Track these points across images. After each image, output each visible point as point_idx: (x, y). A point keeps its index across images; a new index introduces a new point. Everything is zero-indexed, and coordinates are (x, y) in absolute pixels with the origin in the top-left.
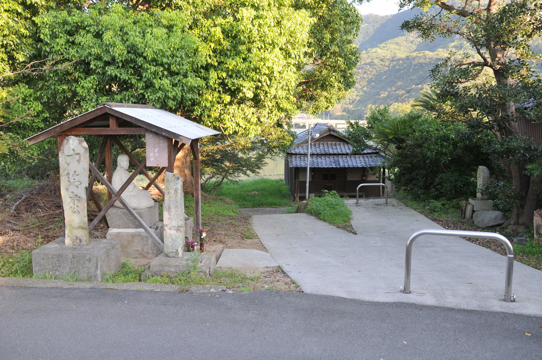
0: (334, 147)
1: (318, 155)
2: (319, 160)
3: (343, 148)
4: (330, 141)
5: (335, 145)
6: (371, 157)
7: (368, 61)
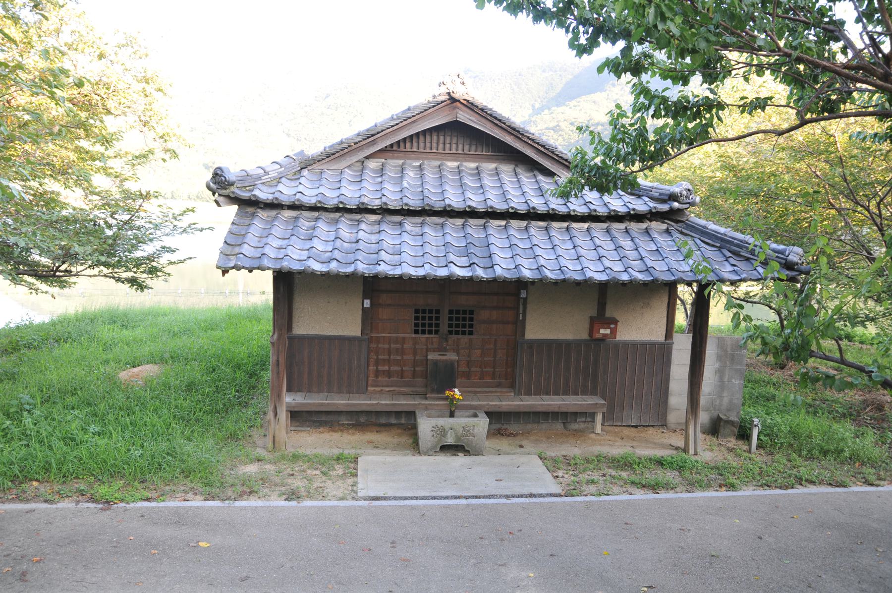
0: (469, 181)
1: (385, 211)
2: (389, 235)
3: (508, 187)
4: (454, 156)
5: (478, 173)
6: (647, 232)
7: (552, 125)
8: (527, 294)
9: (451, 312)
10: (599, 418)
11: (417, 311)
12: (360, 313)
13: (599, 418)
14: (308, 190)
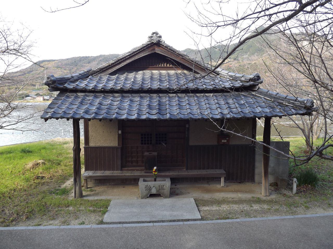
8: (189, 126)
9: (156, 135)
10: (222, 180)
11: (142, 135)
12: (117, 136)
13: (222, 180)
14: (91, 84)
